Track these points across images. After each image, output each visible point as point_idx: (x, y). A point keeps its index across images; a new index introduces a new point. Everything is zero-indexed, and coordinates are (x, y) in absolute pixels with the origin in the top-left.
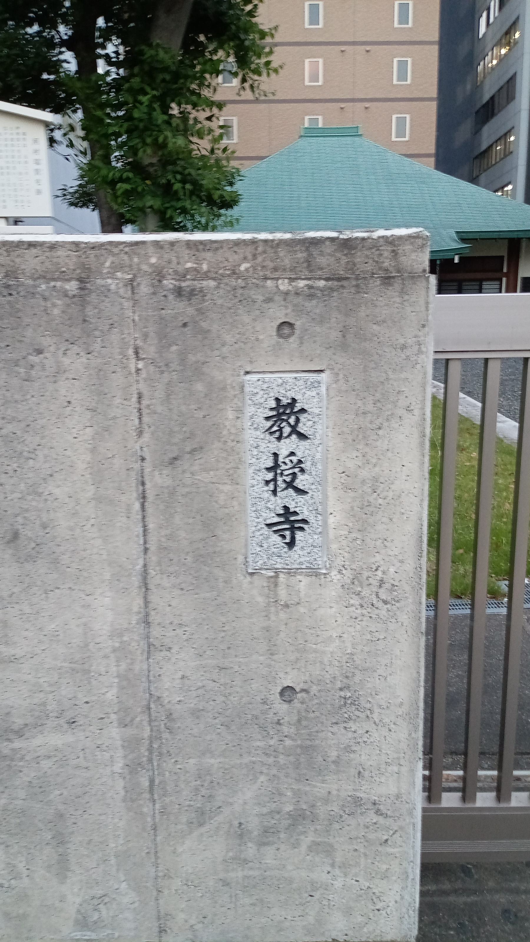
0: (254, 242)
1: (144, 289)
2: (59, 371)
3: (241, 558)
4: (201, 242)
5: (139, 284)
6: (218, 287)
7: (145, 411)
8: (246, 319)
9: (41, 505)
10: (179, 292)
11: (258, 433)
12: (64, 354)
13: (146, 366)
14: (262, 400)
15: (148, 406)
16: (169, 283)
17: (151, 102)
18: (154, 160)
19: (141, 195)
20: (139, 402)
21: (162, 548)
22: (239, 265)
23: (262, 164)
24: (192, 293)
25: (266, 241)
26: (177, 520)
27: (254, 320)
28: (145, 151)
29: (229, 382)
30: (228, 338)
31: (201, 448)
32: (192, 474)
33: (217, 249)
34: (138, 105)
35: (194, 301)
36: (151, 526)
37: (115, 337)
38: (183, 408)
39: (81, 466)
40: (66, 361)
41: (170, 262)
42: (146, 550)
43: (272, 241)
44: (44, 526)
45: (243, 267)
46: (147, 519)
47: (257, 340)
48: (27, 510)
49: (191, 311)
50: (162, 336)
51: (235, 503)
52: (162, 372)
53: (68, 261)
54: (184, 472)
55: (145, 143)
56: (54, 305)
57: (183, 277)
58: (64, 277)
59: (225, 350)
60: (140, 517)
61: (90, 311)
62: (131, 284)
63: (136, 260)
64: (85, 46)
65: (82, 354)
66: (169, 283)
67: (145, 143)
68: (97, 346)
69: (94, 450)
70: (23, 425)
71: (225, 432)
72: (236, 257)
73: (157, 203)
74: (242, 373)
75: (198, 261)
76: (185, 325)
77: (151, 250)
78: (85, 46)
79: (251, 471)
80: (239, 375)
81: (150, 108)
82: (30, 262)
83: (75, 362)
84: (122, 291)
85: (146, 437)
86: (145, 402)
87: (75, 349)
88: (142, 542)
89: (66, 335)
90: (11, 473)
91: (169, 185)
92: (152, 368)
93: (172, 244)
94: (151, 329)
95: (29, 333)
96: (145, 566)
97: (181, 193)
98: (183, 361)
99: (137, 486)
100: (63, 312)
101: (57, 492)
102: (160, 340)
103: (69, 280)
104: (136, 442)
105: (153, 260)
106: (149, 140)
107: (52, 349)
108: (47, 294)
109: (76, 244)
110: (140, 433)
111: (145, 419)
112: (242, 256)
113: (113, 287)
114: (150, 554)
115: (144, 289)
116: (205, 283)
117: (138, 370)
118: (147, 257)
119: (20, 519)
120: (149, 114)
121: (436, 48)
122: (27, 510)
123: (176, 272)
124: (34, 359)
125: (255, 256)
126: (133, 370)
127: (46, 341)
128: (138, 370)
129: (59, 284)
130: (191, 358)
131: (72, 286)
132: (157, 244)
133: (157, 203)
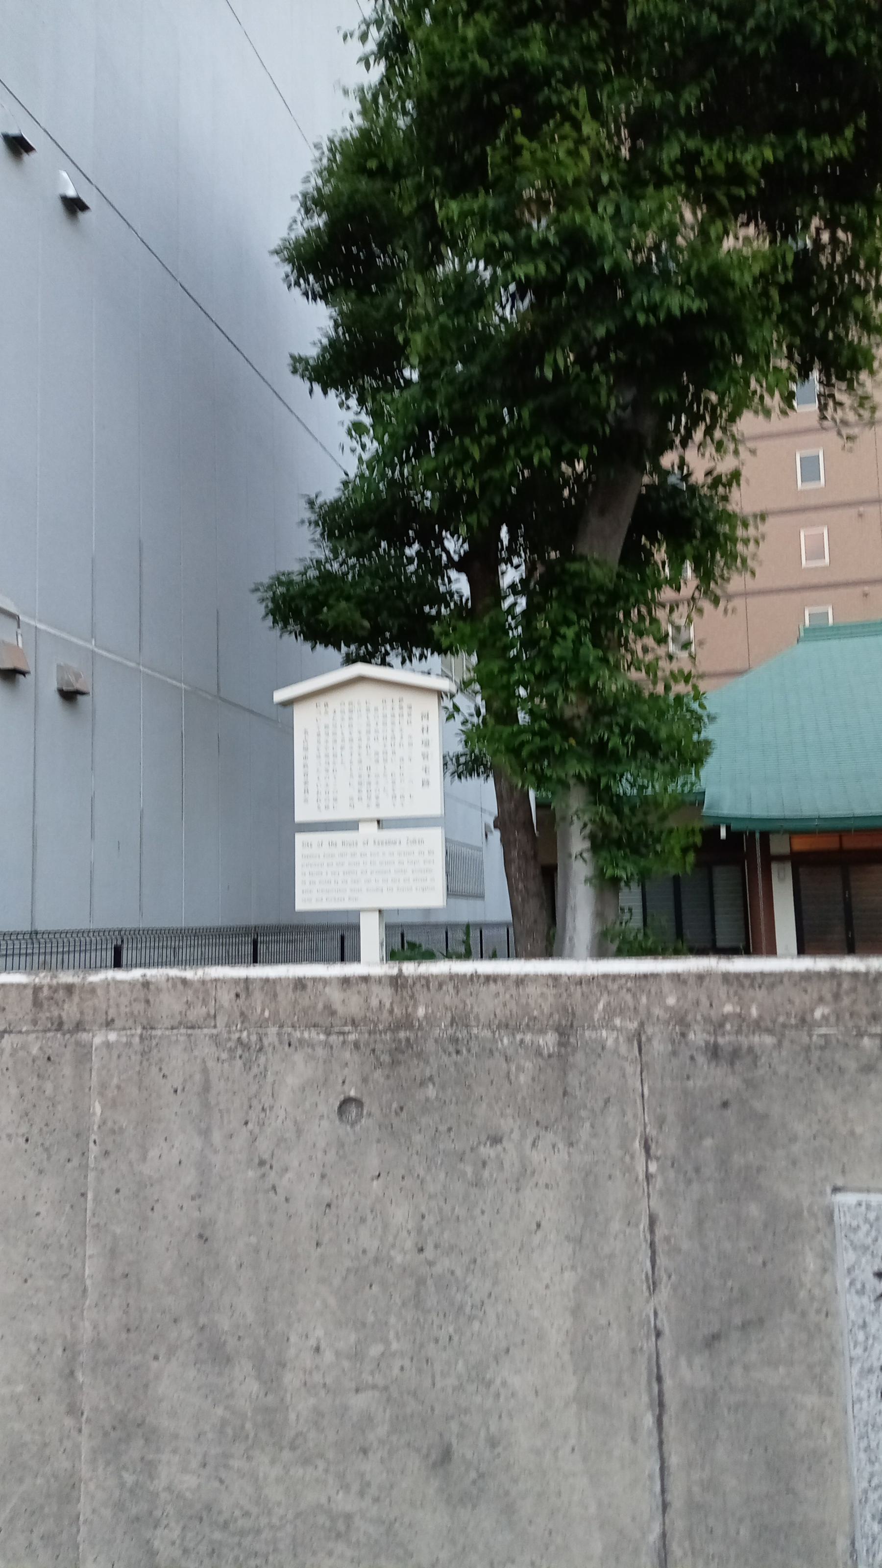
0: (833, 974)
1: (658, 1046)
2: (525, 1171)
3: (842, 1543)
4: (749, 976)
5: (649, 1040)
6: (780, 1044)
7: (660, 1248)
8: (829, 1097)
9: (489, 1403)
10: (714, 1052)
11: (865, 1300)
12: (534, 1144)
13: (662, 1169)
14: (869, 1241)
15: (667, 1239)
16: (698, 1036)
17: (578, 636)
18: (582, 710)
19: (561, 758)
20: (652, 1231)
21: (693, 1507)
22: (812, 1011)
23: (740, 683)
24: (735, 1054)
25: (855, 975)
26: (721, 1453)
27: (844, 1101)
28: (566, 699)
29: (806, 1204)
30: (799, 1128)
31: (761, 1321)
32: (746, 1368)
33: (772, 986)
34: (559, 639)
35: (738, 1066)
36: (674, 1460)
37: (612, 1120)
38: (727, 1246)
39: (555, 1337)
40: (536, 1157)
41: (698, 1003)
42: (665, 1506)
43: (867, 974)
44: (493, 1443)
45: (818, 1014)
46: (665, 1447)
47: (852, 1133)
48: (466, 1411)
49: (733, 1082)
50: (688, 1121)
51: (828, 1432)
52: (689, 1182)
53: (542, 1002)
54: (731, 1363)
55: (566, 687)
56: (520, 1069)
57: (719, 1026)
58: (534, 1025)
59: (796, 1148)
60: (654, 1441)
61: (573, 1079)
62: (638, 1039)
63: (644, 1000)
64: (481, 564)
65: (561, 1145)
66: (698, 1036)
67: (566, 687)
68: (585, 1132)
69: (576, 1311)
70: (466, 1259)
71: (803, 1294)
72: (806, 998)
73: (586, 770)
74: (829, 1190)
75: (741, 1002)
76: (725, 1105)
77: (667, 986)
78: (481, 564)
79: (855, 1370)
80: (822, 1193)
81: (578, 641)
82: (487, 1003)
83: (550, 1159)
84: (623, 1049)
85: (664, 1293)
86: (661, 1231)
87: (549, 1137)
88: (658, 1488)
89: (537, 1115)
90: (443, 1340)
91: (601, 745)
92: (671, 1174)
93: (700, 977)
94: (671, 1111)
95: (482, 1110)
96: (664, 1535)
97: (623, 751)
98: (723, 1163)
99: (649, 1383)
100: (533, 1079)
101: (515, 1381)
102: (685, 1127)
103: (542, 1031)
104: (648, 1302)
105: (671, 1001)
106: (573, 684)
107: (516, 1136)
108: (510, 1052)
109: (555, 979)
110: (654, 1286)
111: (662, 1260)
112: (815, 996)
113: (610, 1043)
114: (671, 1513)
115: (658, 1046)
116: (756, 1039)
117: (648, 1177)
118: (661, 996)
119: (454, 1426)
120: (576, 652)
121: (301, 815)
122: (466, 1411)
123: (707, 1020)
124: (487, 1151)
125: (837, 997)
126: (642, 1176)
127: (508, 1124)
128: (648, 1177)
129: (528, 1038)
130: (738, 1160)
131: (549, 1041)
132: (677, 978)
133: (586, 770)
